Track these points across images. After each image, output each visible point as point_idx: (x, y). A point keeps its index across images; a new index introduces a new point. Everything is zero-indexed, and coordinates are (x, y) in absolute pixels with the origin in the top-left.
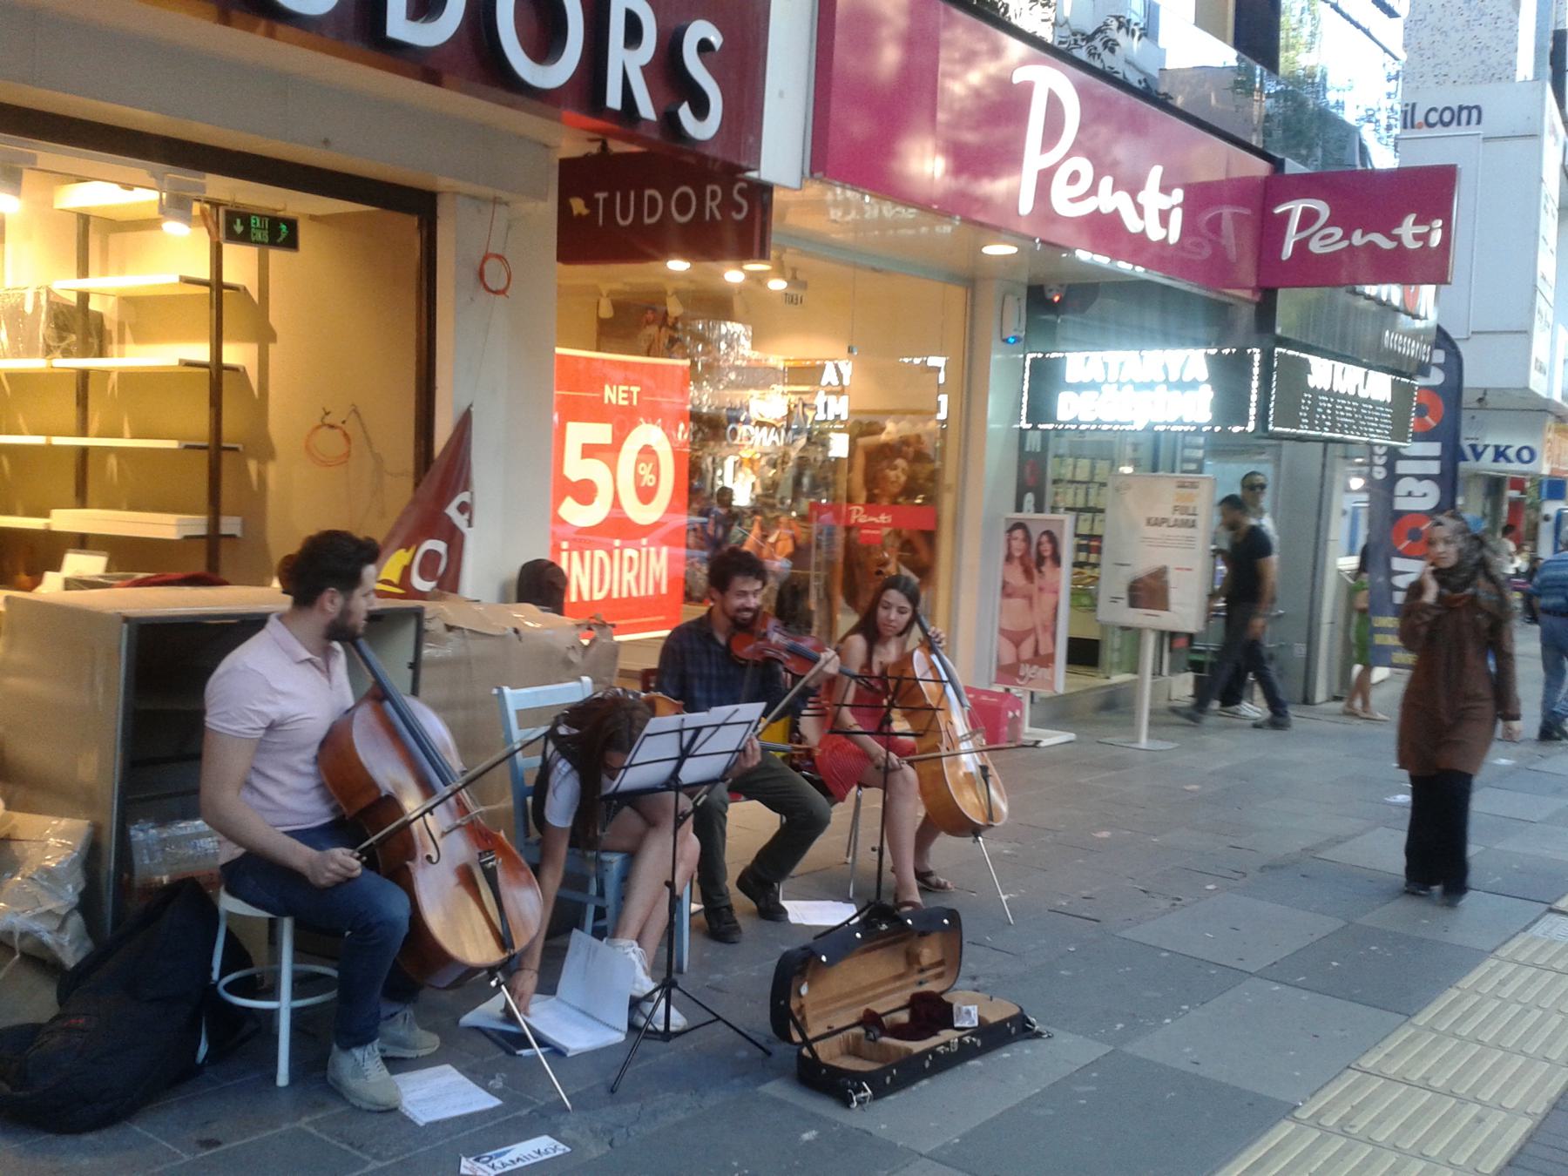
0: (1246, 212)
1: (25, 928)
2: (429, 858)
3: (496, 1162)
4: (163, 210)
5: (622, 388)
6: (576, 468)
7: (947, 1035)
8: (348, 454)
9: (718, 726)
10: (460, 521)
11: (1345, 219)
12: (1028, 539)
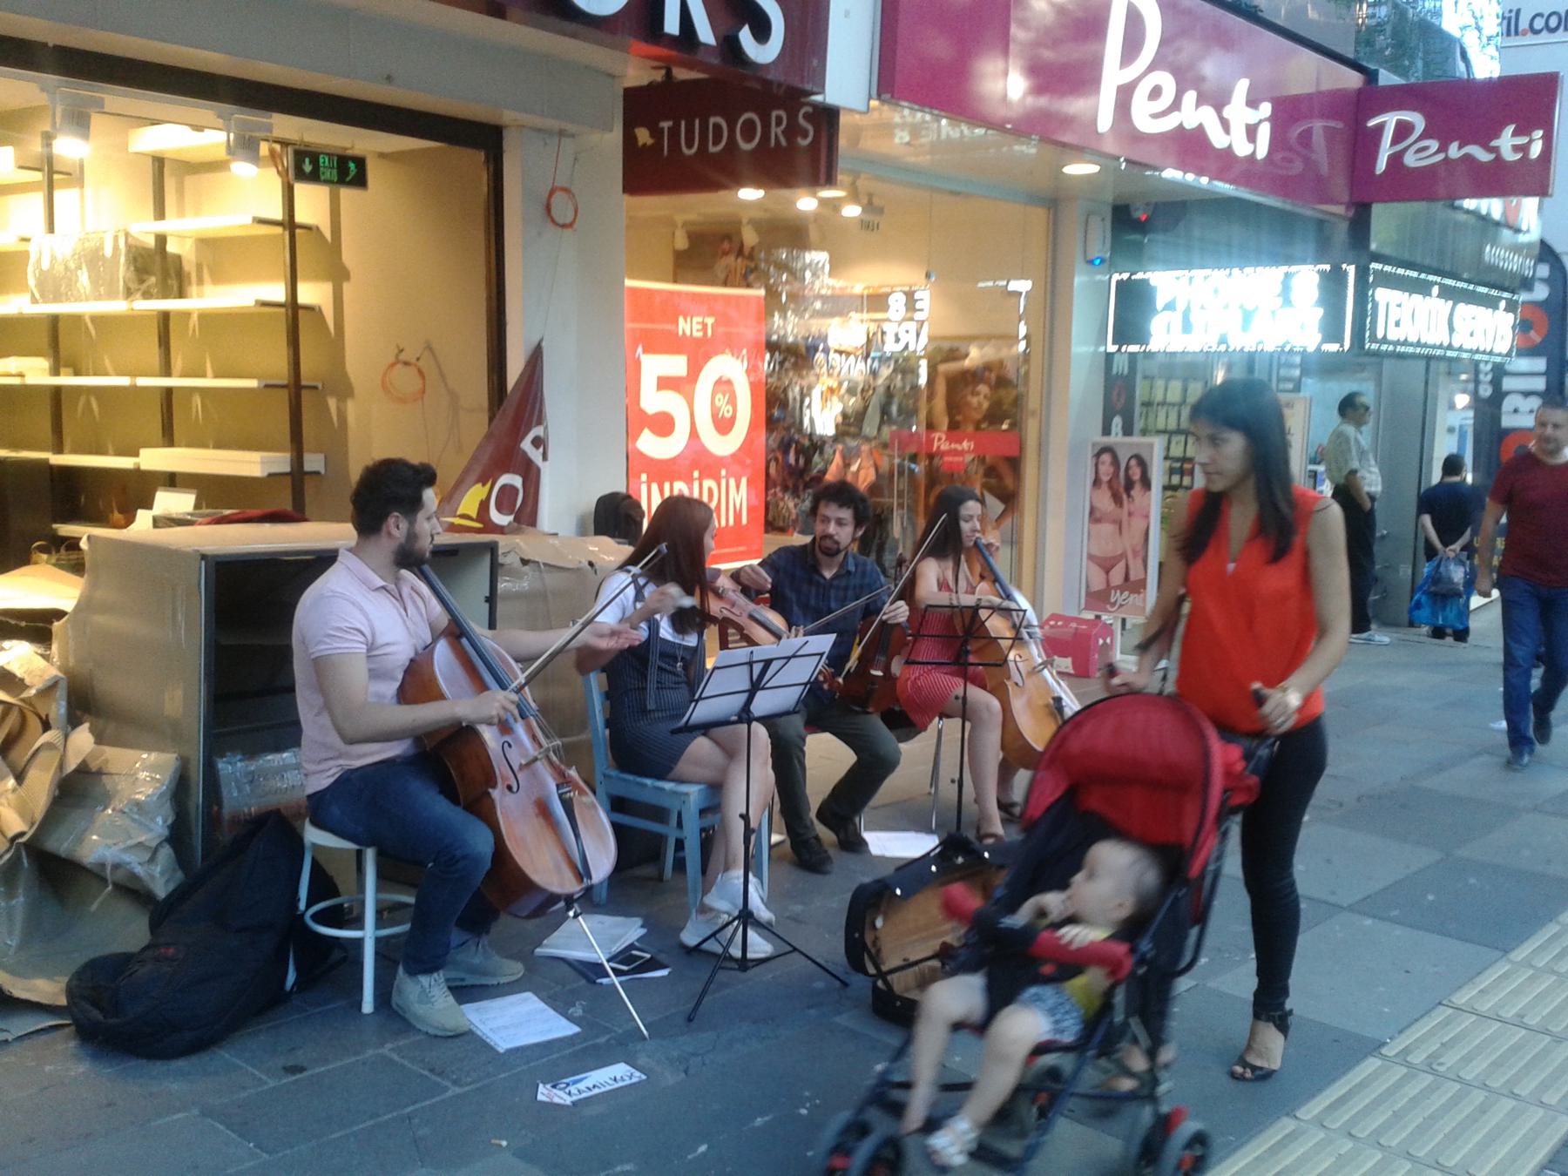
0: (1340, 125)
1: (117, 860)
2: (510, 788)
3: (573, 1089)
6: (652, 400)
9: (789, 658)
10: (535, 455)
11: (1440, 130)
12: (1115, 462)
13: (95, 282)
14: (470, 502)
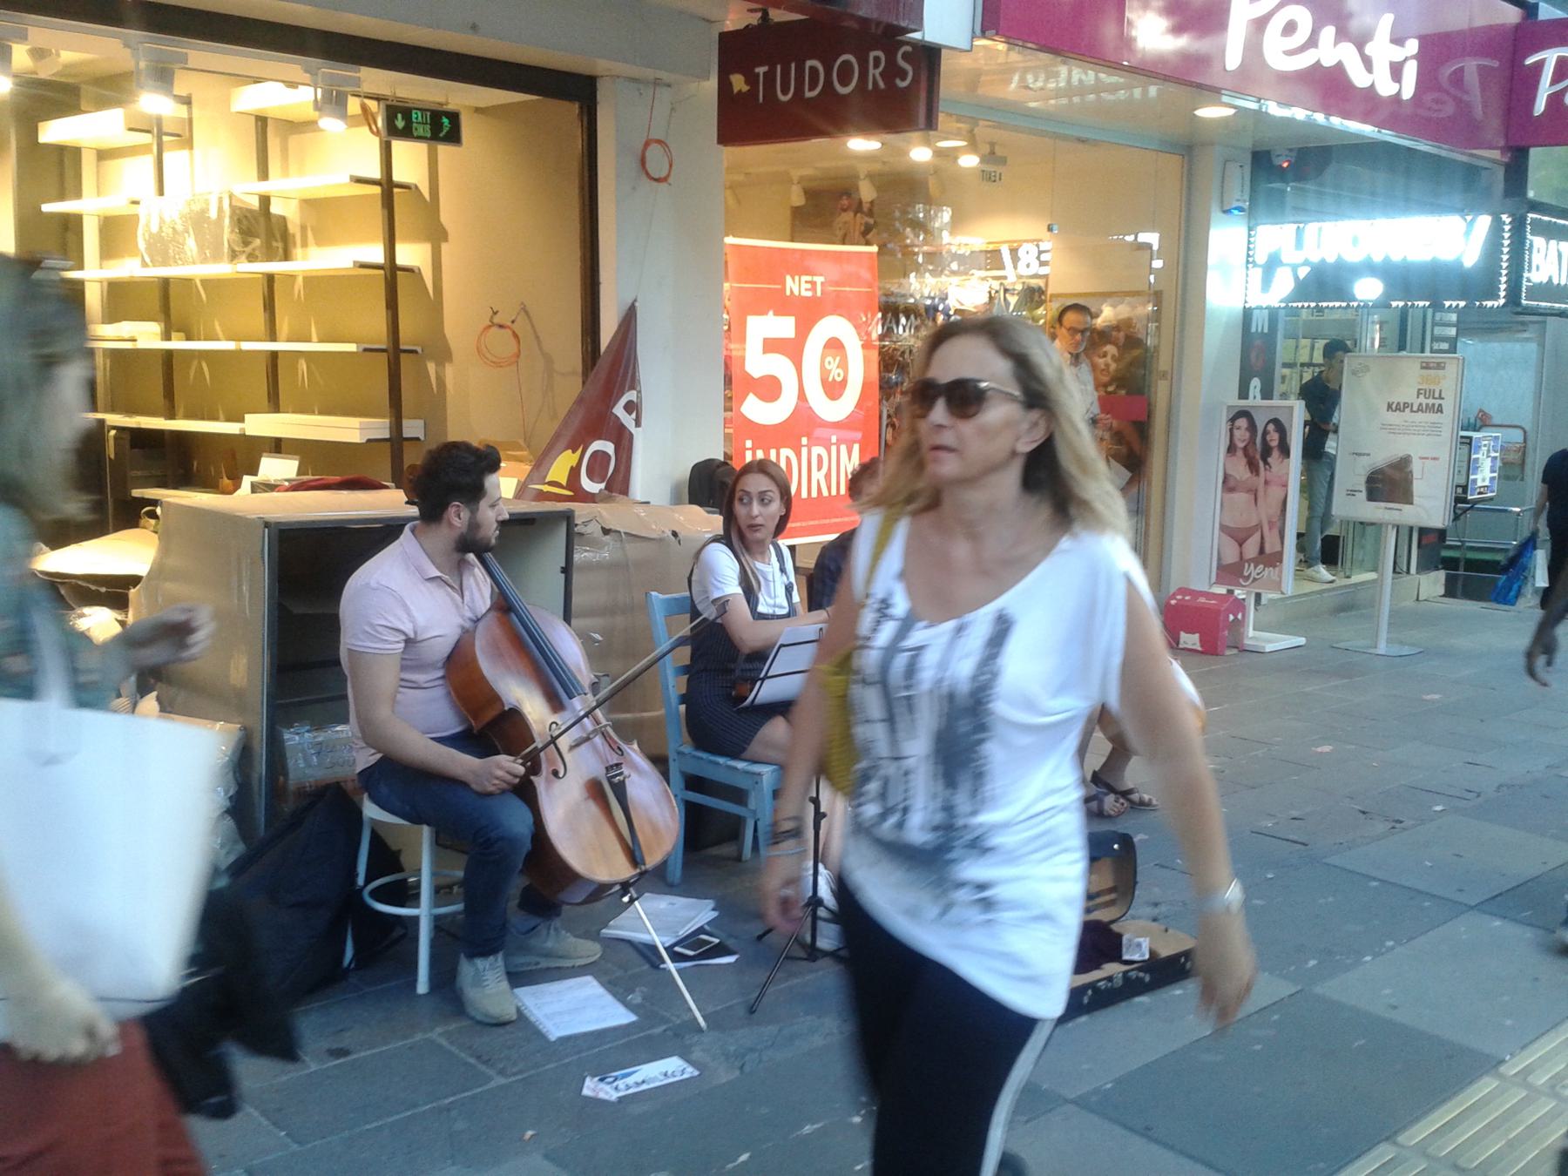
0: (1496, 64)
3: (621, 1084)
4: (317, 106)
5: (804, 278)
6: (757, 363)
7: (1112, 969)
8: (518, 355)
10: (628, 420)
12: (1252, 427)
13: (201, 247)
14: (559, 470)
